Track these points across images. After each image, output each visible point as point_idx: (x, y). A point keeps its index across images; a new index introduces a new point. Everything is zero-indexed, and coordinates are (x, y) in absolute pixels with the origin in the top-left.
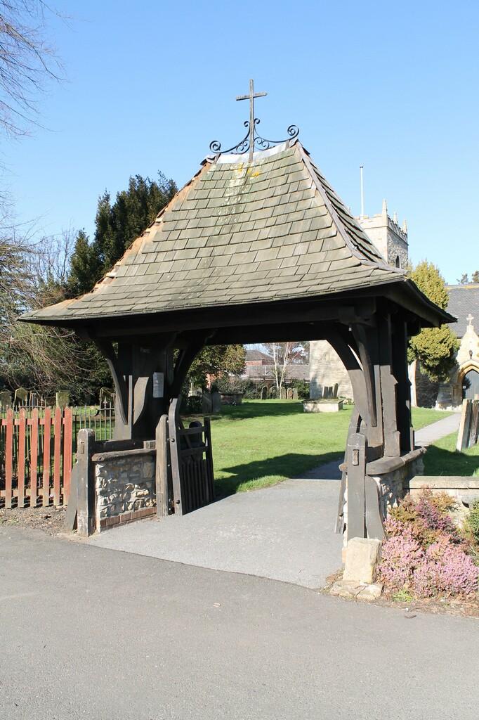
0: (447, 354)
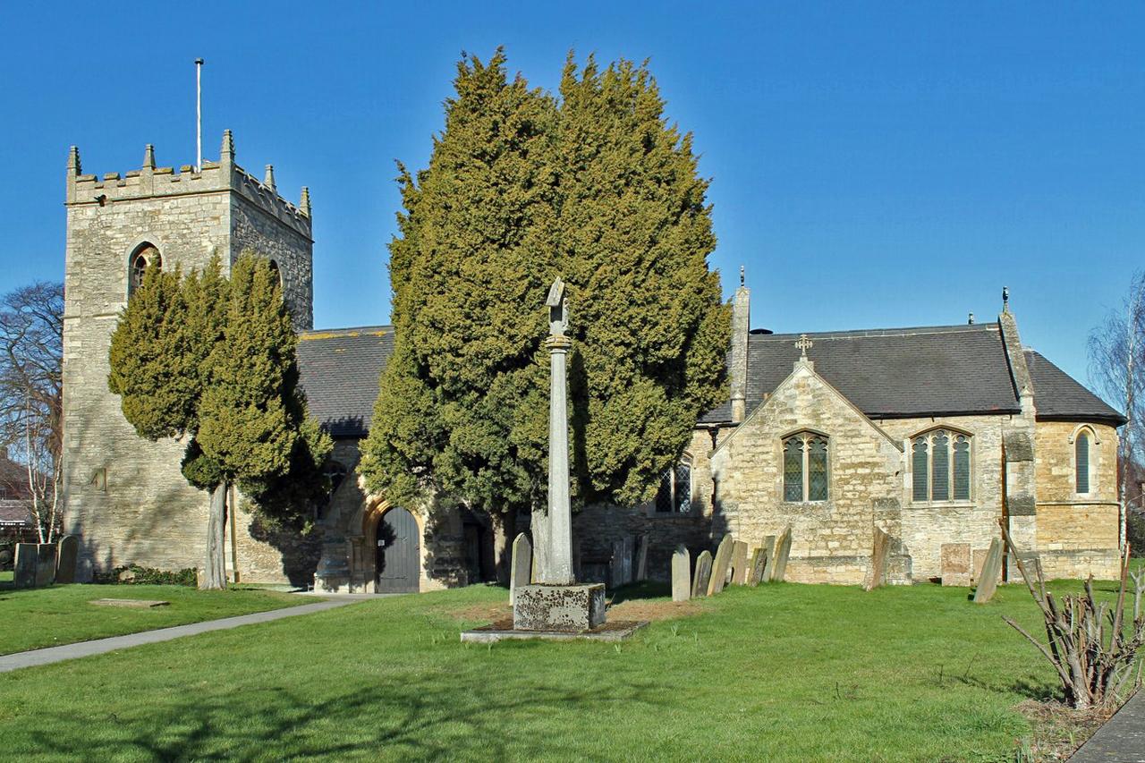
0: (281, 468)
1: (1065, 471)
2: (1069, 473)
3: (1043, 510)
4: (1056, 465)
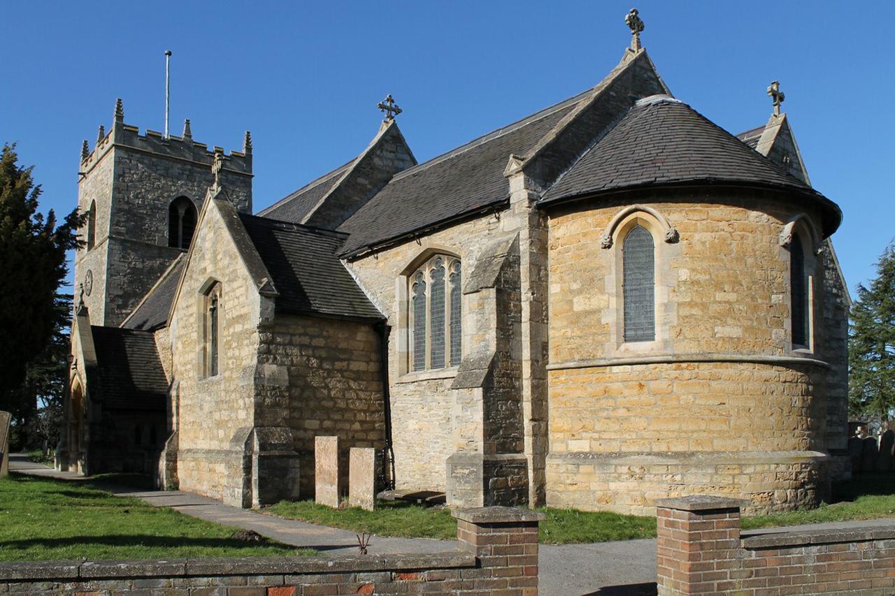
1: (597, 301)
2: (603, 304)
3: (563, 378)
4: (580, 292)
